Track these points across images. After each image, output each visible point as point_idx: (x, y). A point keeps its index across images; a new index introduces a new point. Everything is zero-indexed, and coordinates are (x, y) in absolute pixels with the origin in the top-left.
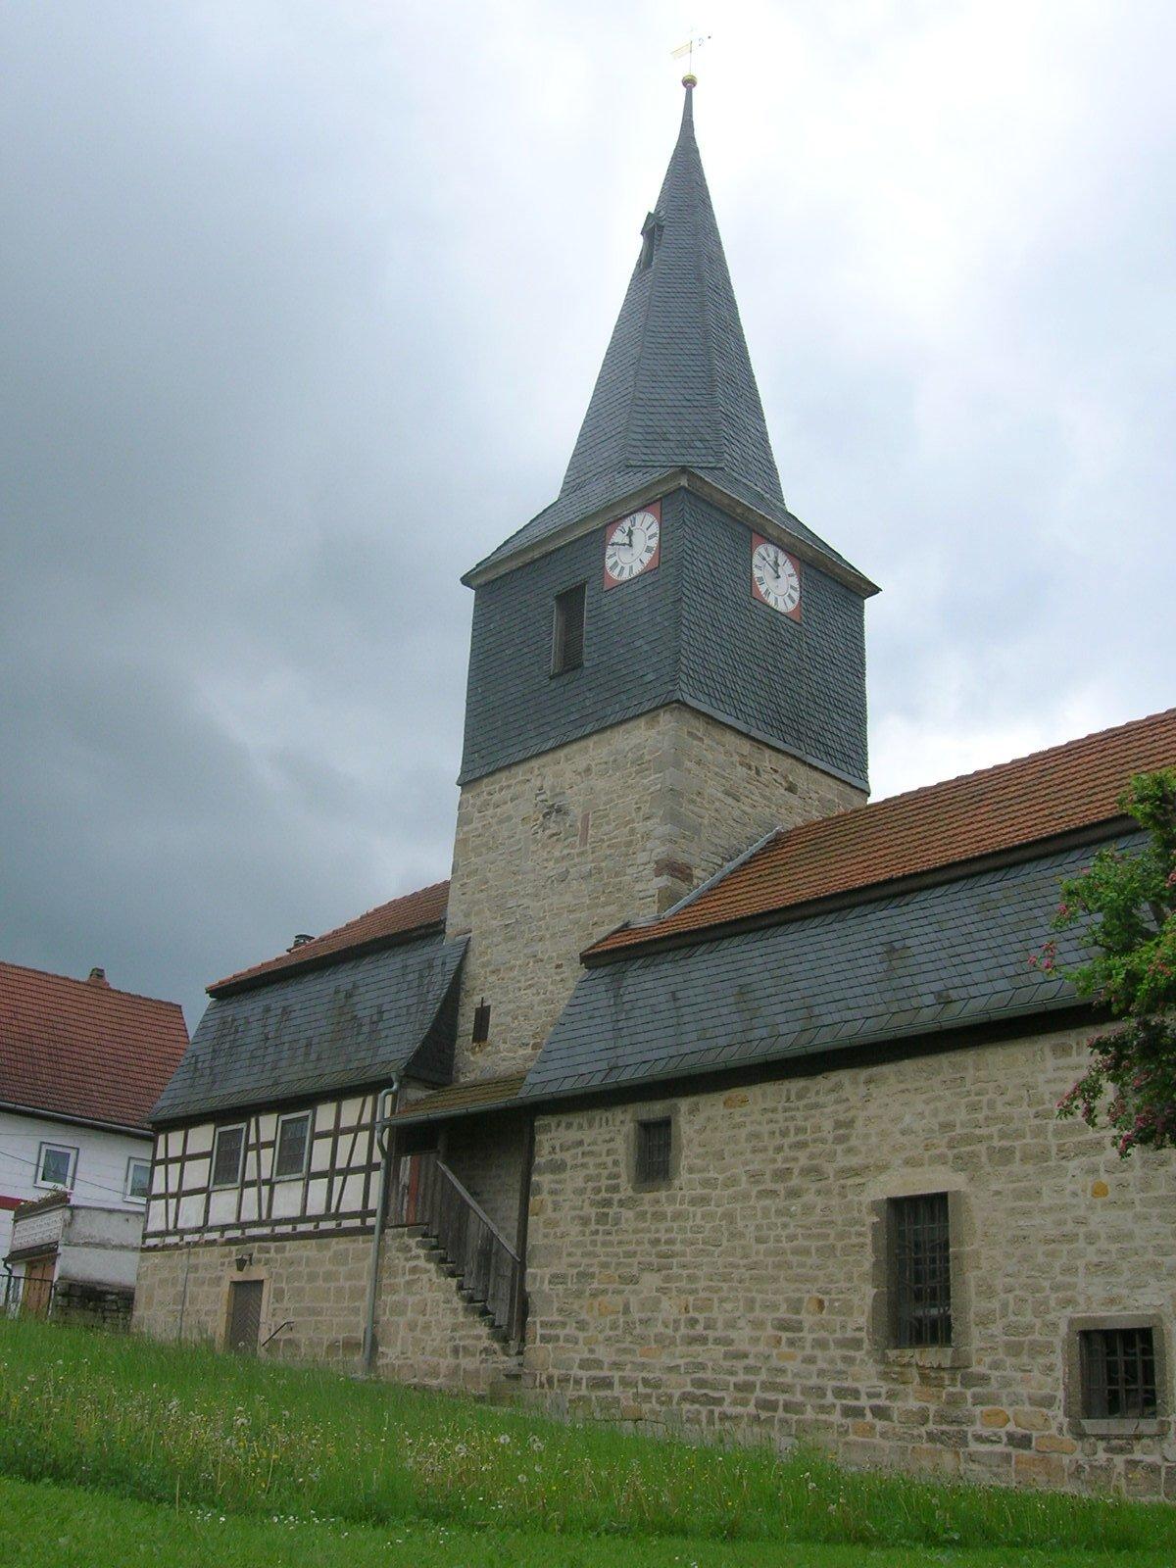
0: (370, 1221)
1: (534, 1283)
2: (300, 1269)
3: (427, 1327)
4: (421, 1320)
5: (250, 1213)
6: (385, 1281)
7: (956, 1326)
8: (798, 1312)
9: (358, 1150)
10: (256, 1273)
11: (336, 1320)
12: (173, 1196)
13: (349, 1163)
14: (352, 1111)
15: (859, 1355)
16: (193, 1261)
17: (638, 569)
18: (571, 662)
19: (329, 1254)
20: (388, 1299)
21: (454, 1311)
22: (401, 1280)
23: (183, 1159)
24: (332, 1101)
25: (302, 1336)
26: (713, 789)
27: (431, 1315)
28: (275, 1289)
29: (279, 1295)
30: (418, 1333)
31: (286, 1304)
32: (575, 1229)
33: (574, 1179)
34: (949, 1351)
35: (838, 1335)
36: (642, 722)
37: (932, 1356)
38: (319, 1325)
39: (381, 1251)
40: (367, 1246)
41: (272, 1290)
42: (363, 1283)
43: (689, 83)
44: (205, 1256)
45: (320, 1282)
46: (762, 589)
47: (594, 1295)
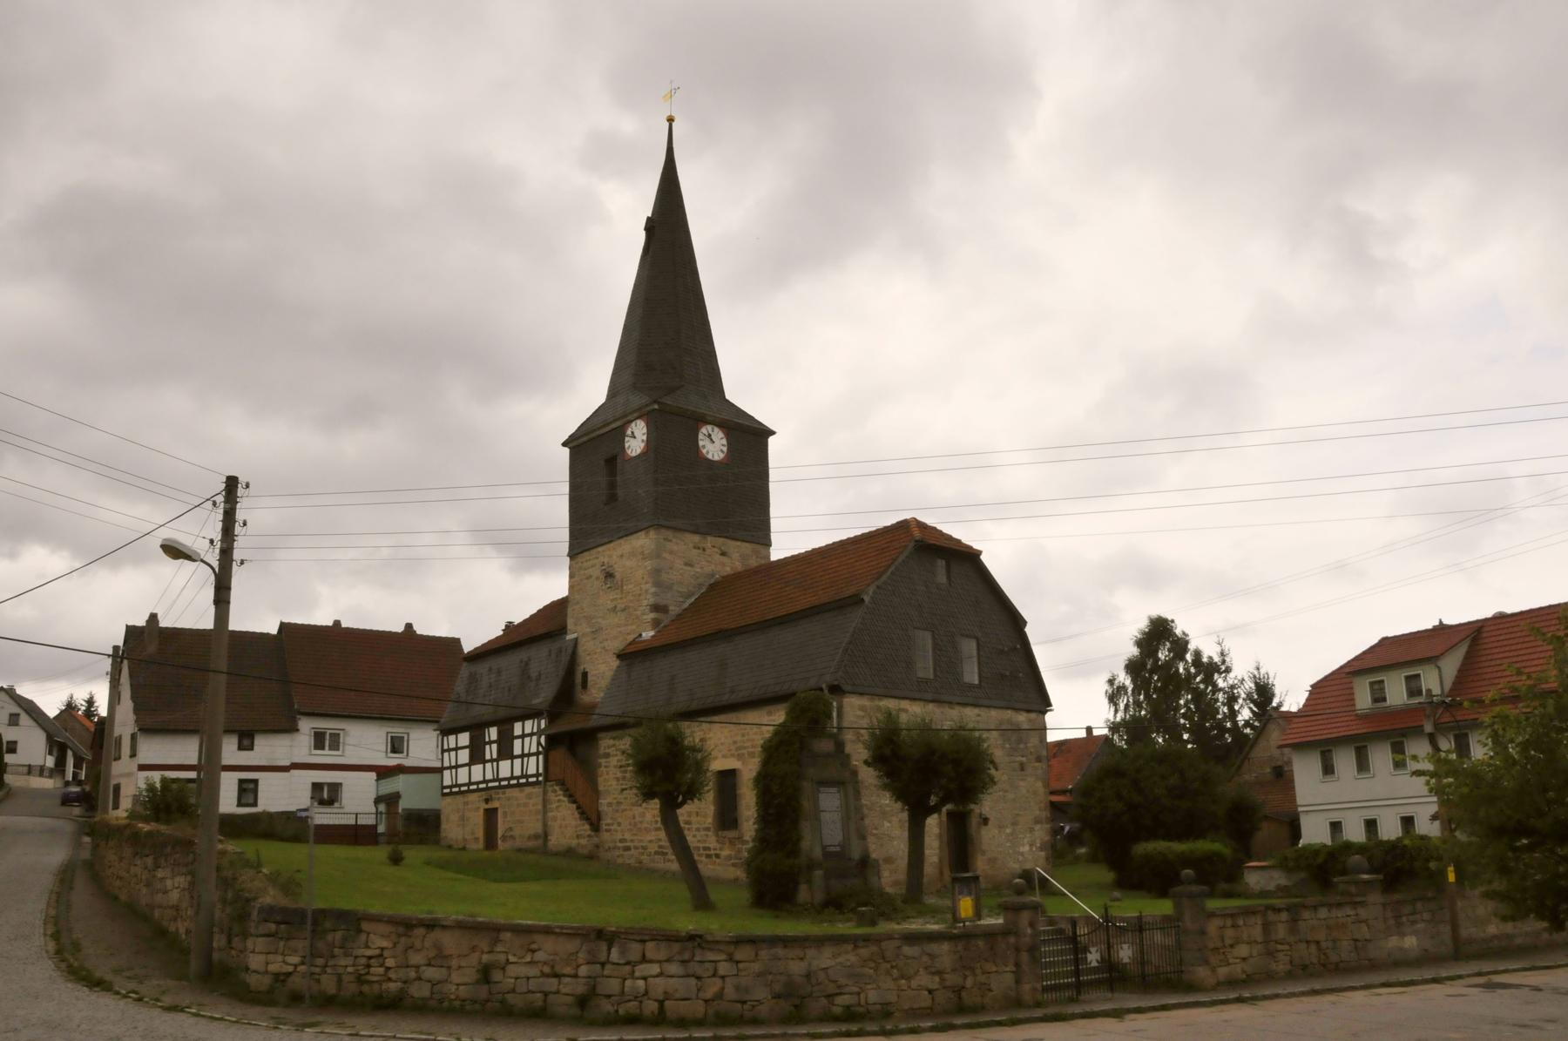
0: (540, 779)
5: (489, 776)
7: (739, 822)
8: (690, 816)
9: (532, 745)
10: (495, 804)
12: (453, 767)
13: (484, 777)
14: (529, 726)
15: (710, 833)
16: (466, 800)
17: (639, 451)
18: (612, 498)
20: (550, 814)
22: (554, 806)
23: (457, 749)
24: (519, 721)
25: (517, 832)
26: (679, 564)
29: (505, 814)
31: (508, 819)
32: (614, 783)
33: (614, 761)
34: (738, 832)
35: (703, 826)
36: (643, 532)
37: (731, 834)
39: (545, 793)
40: (537, 790)
43: (671, 120)
44: (473, 797)
46: (704, 451)
47: (623, 811)
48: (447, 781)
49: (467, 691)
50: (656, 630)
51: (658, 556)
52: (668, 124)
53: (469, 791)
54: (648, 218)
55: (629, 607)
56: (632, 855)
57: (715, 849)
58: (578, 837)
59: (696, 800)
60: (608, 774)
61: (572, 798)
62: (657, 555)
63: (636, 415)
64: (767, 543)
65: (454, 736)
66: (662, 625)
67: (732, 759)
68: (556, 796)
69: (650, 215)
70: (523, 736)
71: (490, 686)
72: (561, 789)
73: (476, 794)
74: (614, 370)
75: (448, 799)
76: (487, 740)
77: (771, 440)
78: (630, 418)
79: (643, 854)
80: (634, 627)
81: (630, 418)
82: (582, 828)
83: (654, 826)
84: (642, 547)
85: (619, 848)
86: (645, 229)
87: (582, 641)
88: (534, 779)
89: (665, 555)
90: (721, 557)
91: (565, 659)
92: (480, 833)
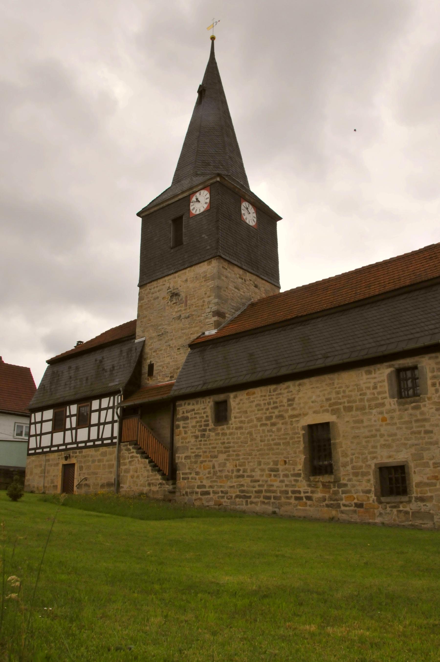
0: (115, 441)
3: (138, 477)
4: (136, 475)
7: (335, 468)
10: (73, 461)
12: (38, 435)
14: (105, 402)
15: (300, 479)
16: (47, 458)
18: (178, 242)
19: (99, 453)
20: (123, 467)
22: (127, 461)
25: (91, 482)
26: (231, 286)
28: (79, 466)
29: (81, 468)
30: (135, 479)
31: (84, 471)
32: (193, 440)
36: (206, 263)
37: (197, 495)
39: (119, 451)
43: (213, 39)
44: (52, 456)
45: (97, 463)
48: (33, 444)
49: (51, 383)
50: (218, 328)
51: (219, 278)
52: (211, 41)
53: (51, 452)
54: (200, 85)
55: (192, 315)
56: (211, 499)
57: (305, 493)
61: (144, 454)
62: (219, 276)
63: (200, 187)
64: (279, 288)
65: (40, 413)
66: (222, 326)
67: (327, 414)
68: (129, 453)
69: (201, 84)
70: (100, 410)
71: (71, 378)
72: (133, 448)
73: (56, 454)
74: (177, 168)
75: (33, 458)
76: (68, 414)
77: (279, 223)
78: (194, 190)
79: (223, 497)
80: (197, 329)
81: (194, 190)
82: (155, 478)
84: (205, 272)
85: (197, 493)
86: (198, 92)
87: (148, 343)
88: (109, 441)
89: (223, 278)
90: (255, 288)
91: (135, 356)
92: (59, 482)
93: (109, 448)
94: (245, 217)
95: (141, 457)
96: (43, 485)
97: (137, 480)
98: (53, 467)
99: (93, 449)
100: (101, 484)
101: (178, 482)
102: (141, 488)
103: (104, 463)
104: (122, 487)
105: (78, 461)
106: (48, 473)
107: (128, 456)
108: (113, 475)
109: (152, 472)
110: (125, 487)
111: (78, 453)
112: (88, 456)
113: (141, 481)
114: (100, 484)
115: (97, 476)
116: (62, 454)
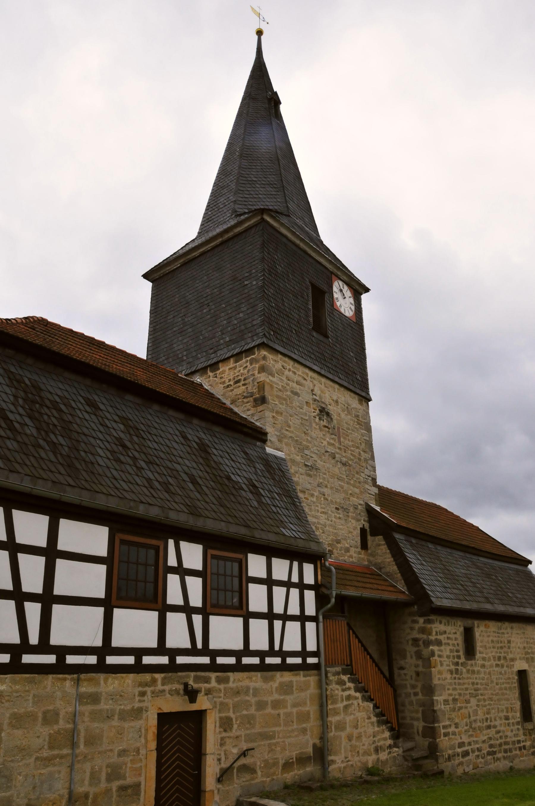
1: (438, 705)
2: (247, 698)
3: (359, 737)
4: (355, 732)
6: (330, 707)
11: (287, 741)
19: (275, 685)
20: (333, 719)
21: (372, 723)
22: (340, 705)
27: (361, 728)
28: (221, 718)
30: (354, 742)
31: (235, 731)
32: (449, 676)
38: (273, 747)
41: (218, 719)
42: (307, 709)
43: (260, 33)
45: (269, 710)
58: (377, 750)
59: (122, 721)
60: (442, 665)
68: (343, 690)
73: (131, 677)
83: (485, 724)
88: (298, 660)
93: (296, 675)
94: (338, 304)
95: (362, 699)
96: (65, 792)
97: (357, 744)
98: (115, 722)
99: (259, 674)
100: (284, 761)
101: (439, 741)
102: (364, 759)
103: (289, 710)
104: (333, 762)
105: (215, 702)
106: (89, 742)
107: (342, 695)
108: (308, 737)
109: (378, 726)
110: (338, 761)
111: (213, 680)
112: (247, 691)
113: (364, 745)
114: (281, 762)
115: (274, 741)
116: (154, 681)
